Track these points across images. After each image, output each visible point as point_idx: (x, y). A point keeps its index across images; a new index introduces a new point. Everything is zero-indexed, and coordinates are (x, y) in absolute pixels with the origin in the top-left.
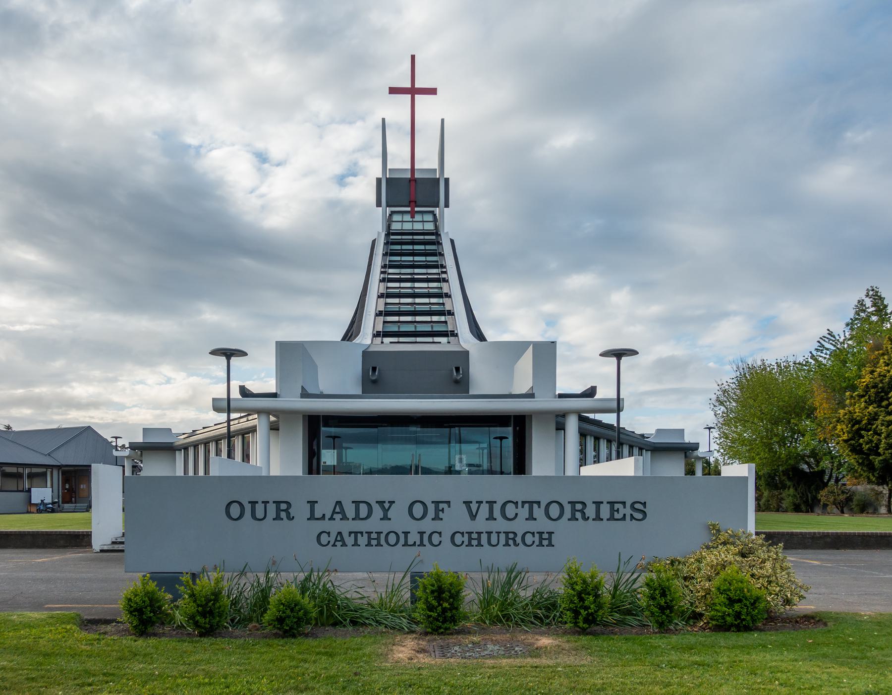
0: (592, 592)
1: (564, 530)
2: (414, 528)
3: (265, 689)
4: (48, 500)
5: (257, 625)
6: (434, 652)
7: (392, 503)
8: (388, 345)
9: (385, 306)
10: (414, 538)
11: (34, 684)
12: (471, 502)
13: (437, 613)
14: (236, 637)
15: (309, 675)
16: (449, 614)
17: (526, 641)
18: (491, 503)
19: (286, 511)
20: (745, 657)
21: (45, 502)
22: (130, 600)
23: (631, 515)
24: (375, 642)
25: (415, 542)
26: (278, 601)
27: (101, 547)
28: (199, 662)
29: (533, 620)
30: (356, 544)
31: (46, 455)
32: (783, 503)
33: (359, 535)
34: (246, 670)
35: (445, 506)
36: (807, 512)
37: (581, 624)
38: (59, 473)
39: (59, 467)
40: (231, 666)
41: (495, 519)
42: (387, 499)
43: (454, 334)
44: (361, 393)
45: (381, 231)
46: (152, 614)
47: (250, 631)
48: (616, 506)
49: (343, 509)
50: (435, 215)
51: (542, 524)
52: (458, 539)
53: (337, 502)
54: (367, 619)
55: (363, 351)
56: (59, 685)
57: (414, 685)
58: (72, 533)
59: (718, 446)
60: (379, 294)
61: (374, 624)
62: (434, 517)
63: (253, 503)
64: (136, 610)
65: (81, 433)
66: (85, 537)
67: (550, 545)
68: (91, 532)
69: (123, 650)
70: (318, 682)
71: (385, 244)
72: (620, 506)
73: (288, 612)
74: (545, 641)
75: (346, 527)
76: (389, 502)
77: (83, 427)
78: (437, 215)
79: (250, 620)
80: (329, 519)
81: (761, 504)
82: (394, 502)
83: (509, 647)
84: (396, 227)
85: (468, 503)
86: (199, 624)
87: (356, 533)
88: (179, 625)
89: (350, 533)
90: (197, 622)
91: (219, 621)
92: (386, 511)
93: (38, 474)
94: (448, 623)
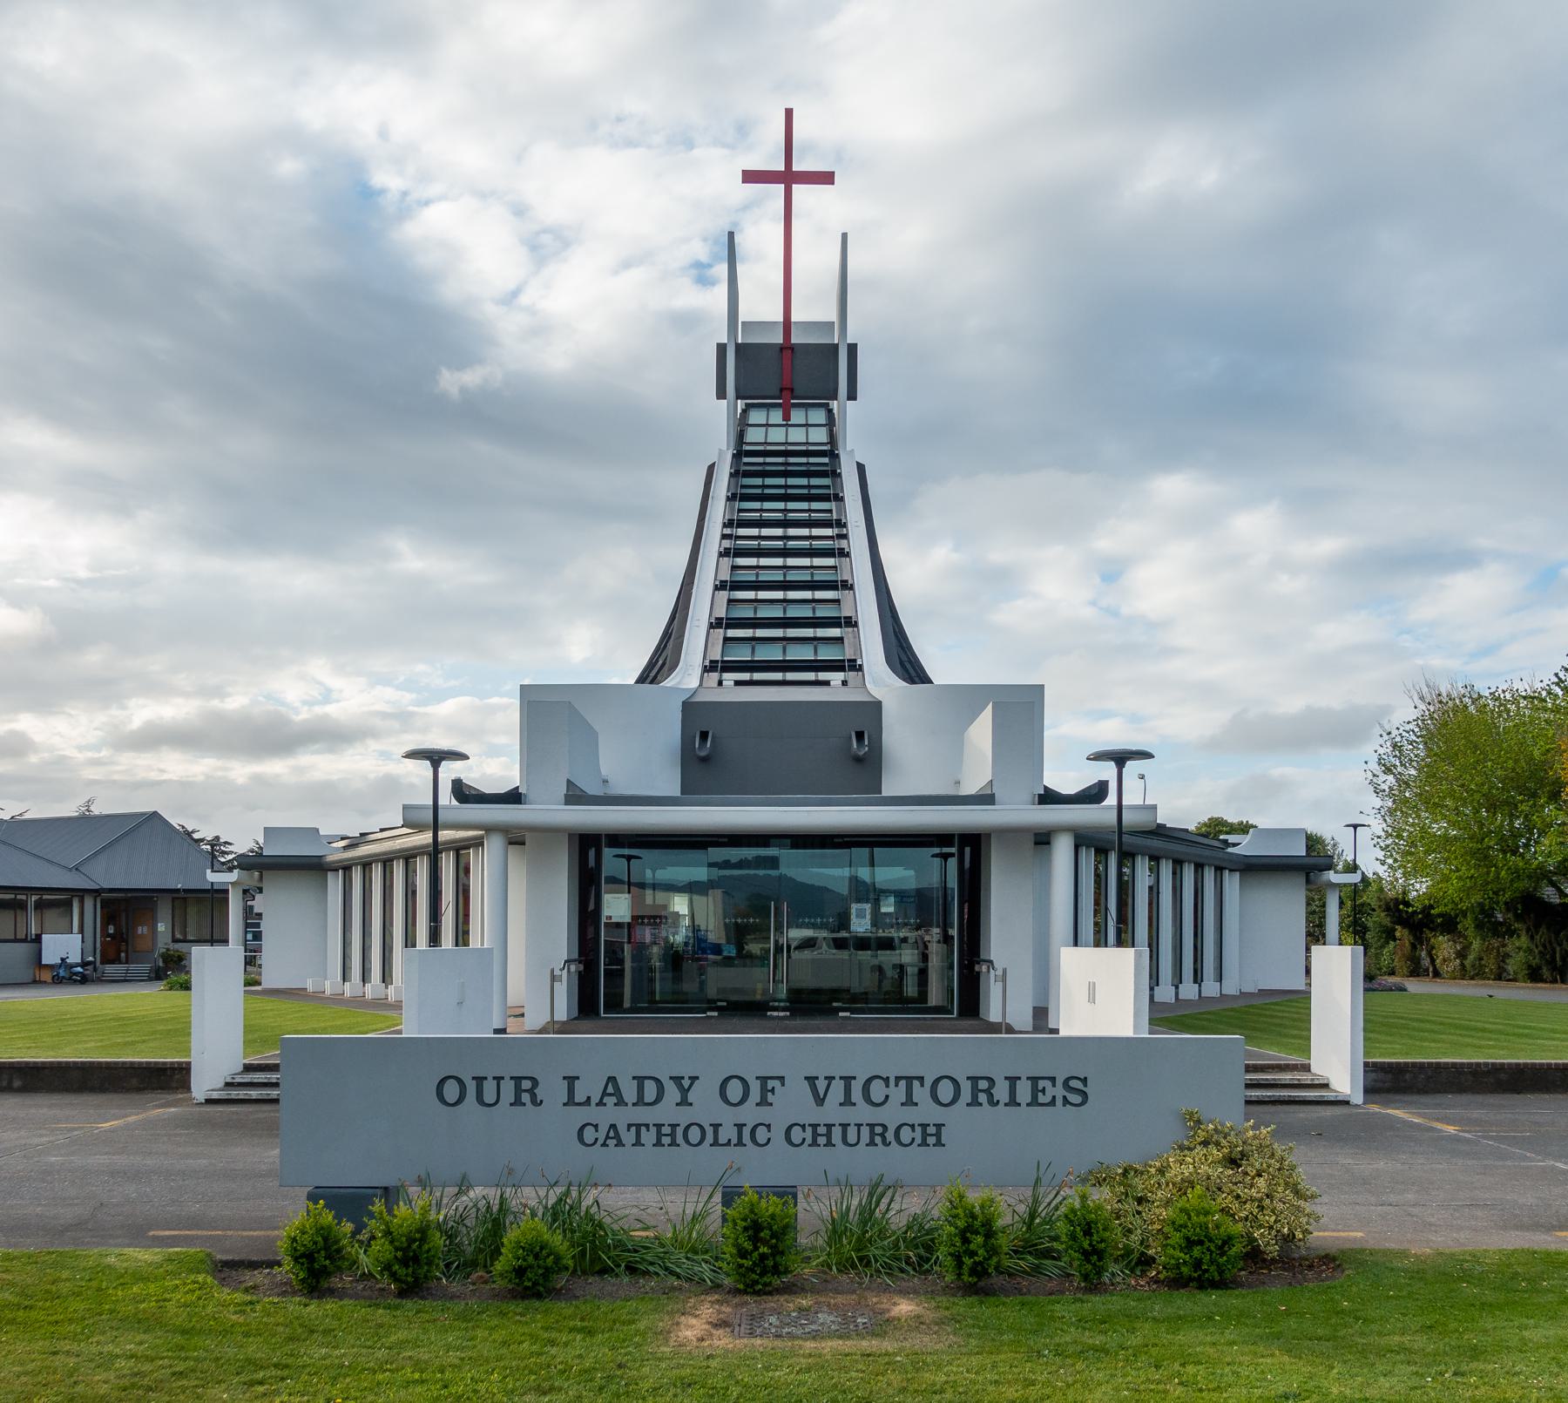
0: (981, 1230)
1: (959, 1120)
2: (728, 1117)
3: (495, 1391)
4: (75, 958)
5: (484, 1274)
6: (740, 1325)
7: (694, 1079)
8: (729, 690)
9: (732, 570)
10: (728, 1133)
11: (185, 1382)
12: (817, 1078)
13: (751, 1260)
14: (453, 1297)
15: (556, 1367)
16: (770, 1263)
17: (878, 1306)
18: (848, 1080)
19: (531, 1092)
20: (1166, 1338)
21: (68, 961)
22: (294, 1240)
23: (1065, 1097)
24: (656, 1310)
25: (730, 1140)
26: (516, 1243)
27: (207, 1095)
28: (402, 1344)
29: (904, 1265)
30: (638, 1143)
31: (70, 870)
32: (1508, 965)
33: (643, 1129)
34: (470, 1358)
35: (776, 1083)
36: (1554, 981)
37: (966, 1278)
38: (95, 901)
39: (96, 893)
40: (448, 1352)
41: (855, 1104)
42: (686, 1072)
43: (854, 666)
44: (679, 795)
45: (724, 447)
46: (328, 1262)
47: (474, 1284)
48: (1041, 1084)
49: (619, 1088)
50: (830, 412)
51: (926, 1111)
52: (797, 1134)
53: (609, 1078)
54: (652, 1264)
55: (683, 702)
56: (219, 1382)
57: (696, 1383)
58: (152, 1066)
59: (1383, 853)
60: (718, 583)
61: (662, 1273)
62: (759, 1101)
63: (480, 1080)
64: (303, 1256)
65: (139, 826)
66: (176, 1072)
67: (939, 1143)
68: (190, 1062)
69: (291, 1322)
70: (567, 1379)
71: (731, 475)
72: (1047, 1084)
73: (531, 1259)
74: (904, 1307)
75: (623, 1117)
76: (690, 1078)
77: (142, 814)
78: (835, 411)
79: (474, 1264)
80: (597, 1105)
81: (1467, 966)
82: (697, 1078)
83: (849, 1317)
84: (754, 436)
85: (811, 1080)
86: (398, 1276)
87: (638, 1126)
88: (364, 1273)
89: (630, 1126)
90: (395, 1273)
91: (428, 1271)
92: (684, 1092)
93: (56, 902)
94: (769, 1275)
